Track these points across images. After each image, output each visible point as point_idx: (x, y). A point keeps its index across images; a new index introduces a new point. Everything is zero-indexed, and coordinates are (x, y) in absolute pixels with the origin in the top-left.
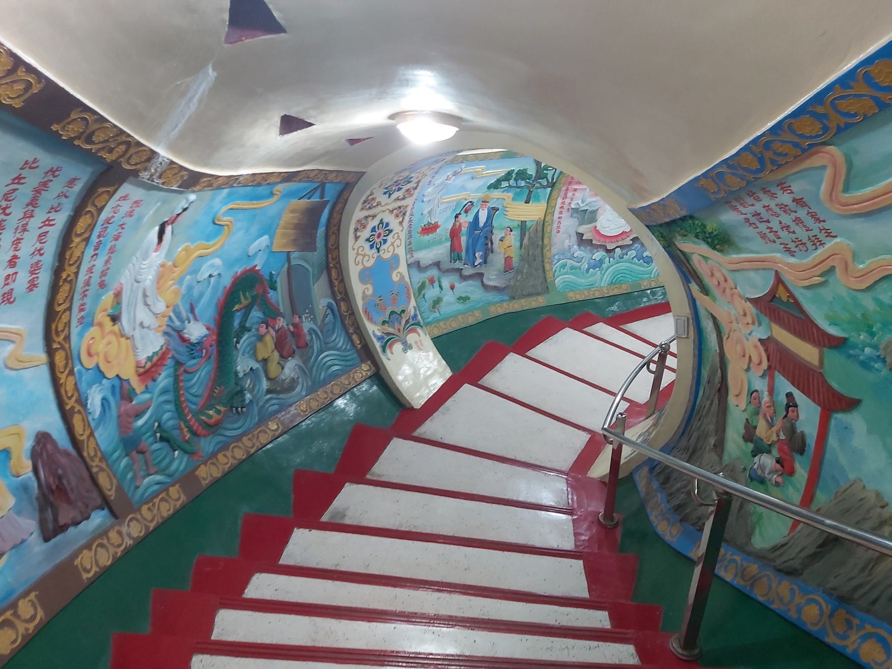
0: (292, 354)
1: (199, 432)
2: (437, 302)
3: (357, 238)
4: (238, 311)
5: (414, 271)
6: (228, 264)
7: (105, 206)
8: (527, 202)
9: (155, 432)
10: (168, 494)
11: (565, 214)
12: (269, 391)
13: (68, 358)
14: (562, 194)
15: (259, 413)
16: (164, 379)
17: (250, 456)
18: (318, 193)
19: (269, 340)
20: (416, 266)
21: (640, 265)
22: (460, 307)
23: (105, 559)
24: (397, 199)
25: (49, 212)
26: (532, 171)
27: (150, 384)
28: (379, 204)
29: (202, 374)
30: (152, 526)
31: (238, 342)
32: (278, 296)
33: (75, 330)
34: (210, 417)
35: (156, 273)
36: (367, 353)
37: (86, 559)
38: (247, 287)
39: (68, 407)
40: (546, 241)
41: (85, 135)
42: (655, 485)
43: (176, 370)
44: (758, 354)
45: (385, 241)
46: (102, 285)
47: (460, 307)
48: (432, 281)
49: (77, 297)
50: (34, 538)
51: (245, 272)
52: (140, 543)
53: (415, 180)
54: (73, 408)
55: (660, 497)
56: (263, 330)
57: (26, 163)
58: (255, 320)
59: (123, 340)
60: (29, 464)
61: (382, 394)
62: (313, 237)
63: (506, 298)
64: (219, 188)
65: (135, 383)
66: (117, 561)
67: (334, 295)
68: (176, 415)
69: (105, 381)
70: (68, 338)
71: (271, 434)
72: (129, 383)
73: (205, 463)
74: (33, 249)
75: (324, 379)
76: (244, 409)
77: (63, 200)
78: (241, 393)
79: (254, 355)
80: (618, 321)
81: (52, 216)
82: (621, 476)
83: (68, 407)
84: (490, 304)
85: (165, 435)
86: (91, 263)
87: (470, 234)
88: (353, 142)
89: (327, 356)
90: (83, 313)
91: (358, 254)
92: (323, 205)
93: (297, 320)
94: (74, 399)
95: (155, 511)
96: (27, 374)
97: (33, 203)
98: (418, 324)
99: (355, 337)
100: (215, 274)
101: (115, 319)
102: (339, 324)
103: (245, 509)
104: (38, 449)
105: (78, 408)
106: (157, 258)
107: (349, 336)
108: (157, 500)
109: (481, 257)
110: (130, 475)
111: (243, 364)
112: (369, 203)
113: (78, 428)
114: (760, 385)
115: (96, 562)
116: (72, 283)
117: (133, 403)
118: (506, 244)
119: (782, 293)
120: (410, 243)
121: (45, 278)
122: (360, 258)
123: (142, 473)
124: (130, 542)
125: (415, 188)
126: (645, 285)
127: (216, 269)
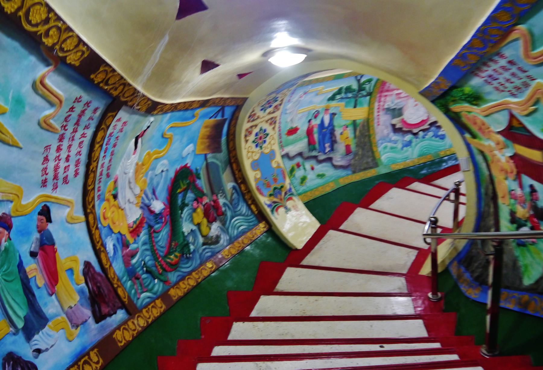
0: (215, 220)
1: (167, 269)
2: (303, 179)
3: (247, 141)
4: (180, 193)
5: (286, 160)
6: (172, 163)
7: (110, 124)
8: (355, 107)
9: (143, 267)
10: (155, 304)
11: (381, 113)
12: (204, 244)
13: (95, 218)
14: (378, 99)
15: (200, 257)
16: (143, 236)
17: (198, 284)
18: (220, 114)
19: (200, 210)
20: (286, 156)
21: (437, 141)
22: (319, 181)
24: (270, 113)
25: (84, 129)
26: (355, 86)
27: (137, 238)
28: (258, 118)
29: (163, 236)
30: (150, 321)
31: (182, 213)
32: (202, 183)
33: (97, 203)
34: (172, 260)
35: (141, 163)
36: (261, 216)
37: (118, 335)
38: (184, 177)
39: (98, 248)
40: (371, 132)
41: (105, 81)
42: (463, 269)
43: (149, 231)
44: (510, 166)
45: (265, 142)
46: (108, 175)
47: (319, 181)
48: (298, 165)
49: (97, 182)
50: (91, 321)
51: (182, 168)
52: (145, 329)
53: (280, 99)
54: (100, 249)
55: (467, 275)
56: (195, 204)
57: (76, 99)
58: (190, 199)
59: (120, 210)
60: (82, 278)
61: (274, 243)
62: (219, 143)
63: (350, 172)
64: (166, 112)
65: (129, 237)
66: (134, 338)
67: (236, 180)
68: (152, 258)
69: (113, 235)
70: (94, 206)
71: (209, 270)
72: (125, 237)
73: (173, 287)
74: (76, 152)
75: (237, 235)
76: (191, 255)
77: (91, 121)
78: (187, 245)
79: (192, 221)
80: (428, 180)
81: (86, 131)
82: (440, 270)
83: (98, 248)
85: (148, 269)
86: (103, 161)
87: (320, 132)
88: (241, 76)
89: (237, 221)
90: (99, 193)
91: (248, 152)
92: (224, 121)
93: (215, 198)
94: (100, 243)
95: (150, 313)
96: (76, 226)
97: (77, 123)
98: (292, 194)
99: (253, 207)
100: (165, 169)
101: (115, 197)
102: (241, 199)
103: (200, 315)
104: (86, 270)
105: (102, 249)
106: (134, 159)
107: (249, 206)
108: (150, 307)
109: (329, 147)
110: (133, 291)
111: (186, 227)
112: (252, 117)
113: (104, 261)
114: (514, 185)
115: (124, 337)
116: (95, 172)
117: (130, 248)
118: (345, 137)
119: (515, 124)
120: (281, 142)
121: (82, 169)
122: (250, 154)
123: (139, 291)
124: (140, 329)
125: (280, 105)
126: (442, 154)
127: (165, 169)
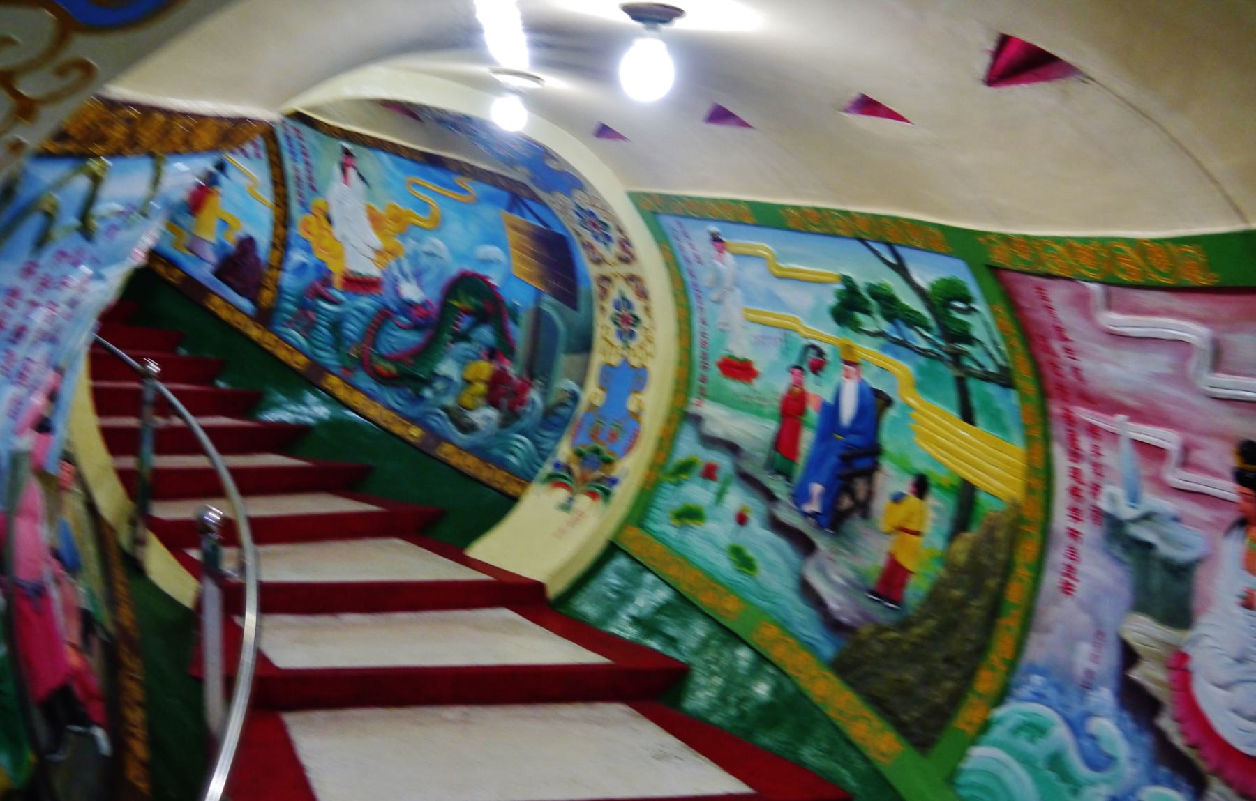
2: (690, 515)
22: (724, 566)
23: (224, 314)
37: (216, 301)
47: (724, 566)
63: (828, 650)
84: (784, 625)
